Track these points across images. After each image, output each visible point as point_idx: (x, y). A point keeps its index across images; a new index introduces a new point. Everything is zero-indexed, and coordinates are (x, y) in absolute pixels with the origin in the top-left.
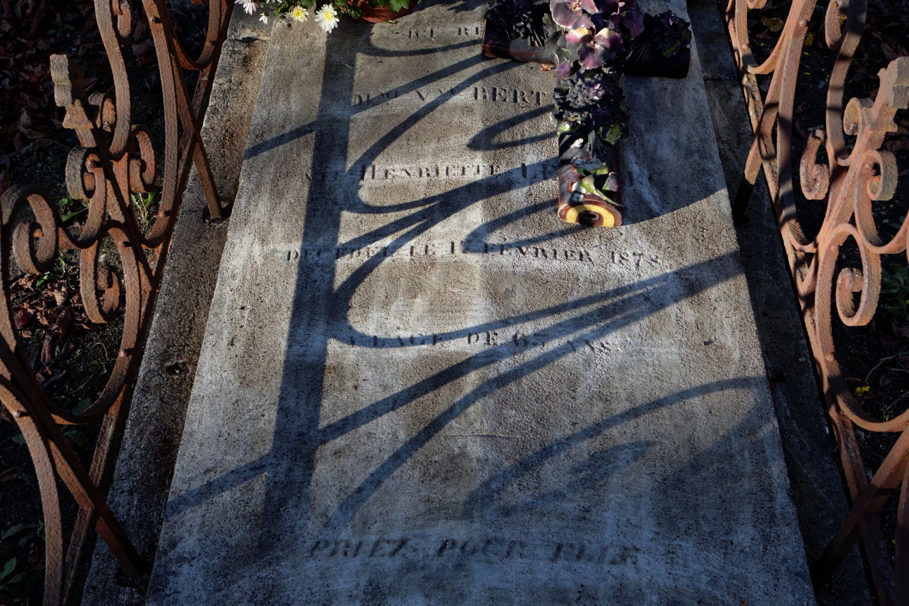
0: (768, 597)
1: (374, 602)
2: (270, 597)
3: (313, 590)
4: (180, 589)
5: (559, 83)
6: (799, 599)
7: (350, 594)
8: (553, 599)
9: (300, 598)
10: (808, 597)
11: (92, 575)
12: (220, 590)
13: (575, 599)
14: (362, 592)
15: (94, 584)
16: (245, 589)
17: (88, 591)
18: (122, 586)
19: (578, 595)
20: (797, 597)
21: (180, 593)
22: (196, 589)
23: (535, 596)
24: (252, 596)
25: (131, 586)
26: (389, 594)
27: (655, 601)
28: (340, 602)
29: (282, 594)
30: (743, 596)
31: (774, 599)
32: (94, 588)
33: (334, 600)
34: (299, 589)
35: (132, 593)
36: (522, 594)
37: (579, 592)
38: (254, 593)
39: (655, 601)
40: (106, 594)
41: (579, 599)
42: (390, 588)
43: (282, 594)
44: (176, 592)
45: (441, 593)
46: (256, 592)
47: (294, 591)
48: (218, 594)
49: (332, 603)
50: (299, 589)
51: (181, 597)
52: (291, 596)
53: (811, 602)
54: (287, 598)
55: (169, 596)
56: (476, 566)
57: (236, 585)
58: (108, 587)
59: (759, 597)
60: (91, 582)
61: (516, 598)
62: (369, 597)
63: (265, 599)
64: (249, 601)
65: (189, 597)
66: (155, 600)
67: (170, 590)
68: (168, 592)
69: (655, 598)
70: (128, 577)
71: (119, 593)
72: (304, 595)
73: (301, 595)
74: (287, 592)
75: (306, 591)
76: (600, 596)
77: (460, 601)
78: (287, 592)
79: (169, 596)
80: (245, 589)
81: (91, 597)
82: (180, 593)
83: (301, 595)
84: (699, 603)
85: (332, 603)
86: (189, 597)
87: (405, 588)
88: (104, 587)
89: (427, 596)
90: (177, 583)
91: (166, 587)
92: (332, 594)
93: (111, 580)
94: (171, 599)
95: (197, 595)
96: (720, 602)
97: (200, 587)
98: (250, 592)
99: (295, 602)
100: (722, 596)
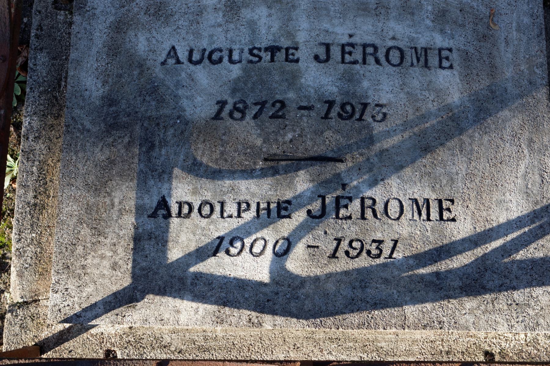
0: (510, 7)
1: (232, 12)
2: (159, 10)
3: (189, 5)
4: (96, 6)
5: (326, 130)
6: (531, 8)
7: (215, 7)
8: (358, 9)
9: (180, 11)
10: (538, 7)
11: (36, 3)
12: (123, 7)
13: (374, 8)
14: (223, 6)
15: (39, 9)
16: (141, 5)
17: (36, 14)
18: (58, 10)
19: (376, 6)
20: (530, 6)
21: (96, 9)
22: (107, 6)
23: (345, 6)
24: (146, 10)
25: (65, 10)
26: (243, 7)
27: (430, 10)
28: (208, 13)
29: (167, 8)
30: (492, 6)
31: (514, 8)
32: (40, 12)
33: (204, 12)
34: (179, 4)
35: (66, 15)
36: (336, 5)
37: (377, 4)
38: (147, 8)
39: (430, 10)
40: (49, 16)
41: (376, 8)
42: (243, 3)
43: (167, 8)
44: (93, 8)
45: (279, 5)
46: (149, 7)
47: (175, 6)
48: (122, 9)
49: (203, 13)
50: (179, 4)
51: (97, 12)
52: (174, 10)
53: (540, 10)
54: (171, 11)
55: (89, 11)
56: (311, 185)
57: (135, 3)
58: (48, 11)
59: (503, 7)
60: (36, 8)
61: (332, 8)
62: (228, 9)
63: (156, 12)
64: (145, 14)
65: (103, 12)
66: (80, 15)
67: (89, 7)
68: (88, 9)
69: (430, 8)
70: (61, 4)
71: (57, 15)
72: (183, 9)
73: (181, 9)
74: (171, 7)
75: (184, 6)
76: (392, 7)
77: (292, 10)
78: (171, 7)
79: (89, 11)
80: (141, 5)
81: (38, 18)
82: (96, 9)
83: (181, 9)
84: (461, 11)
85: (203, 13)
86: (103, 12)
87: (253, 2)
88: (46, 11)
89: (269, 7)
90: (93, 2)
91: (86, 5)
92: (202, 7)
93: (50, 6)
94: (91, 13)
95: (108, 10)
96: (476, 10)
97: (110, 5)
98: (145, 8)
99: (177, 13)
100: (477, 6)
